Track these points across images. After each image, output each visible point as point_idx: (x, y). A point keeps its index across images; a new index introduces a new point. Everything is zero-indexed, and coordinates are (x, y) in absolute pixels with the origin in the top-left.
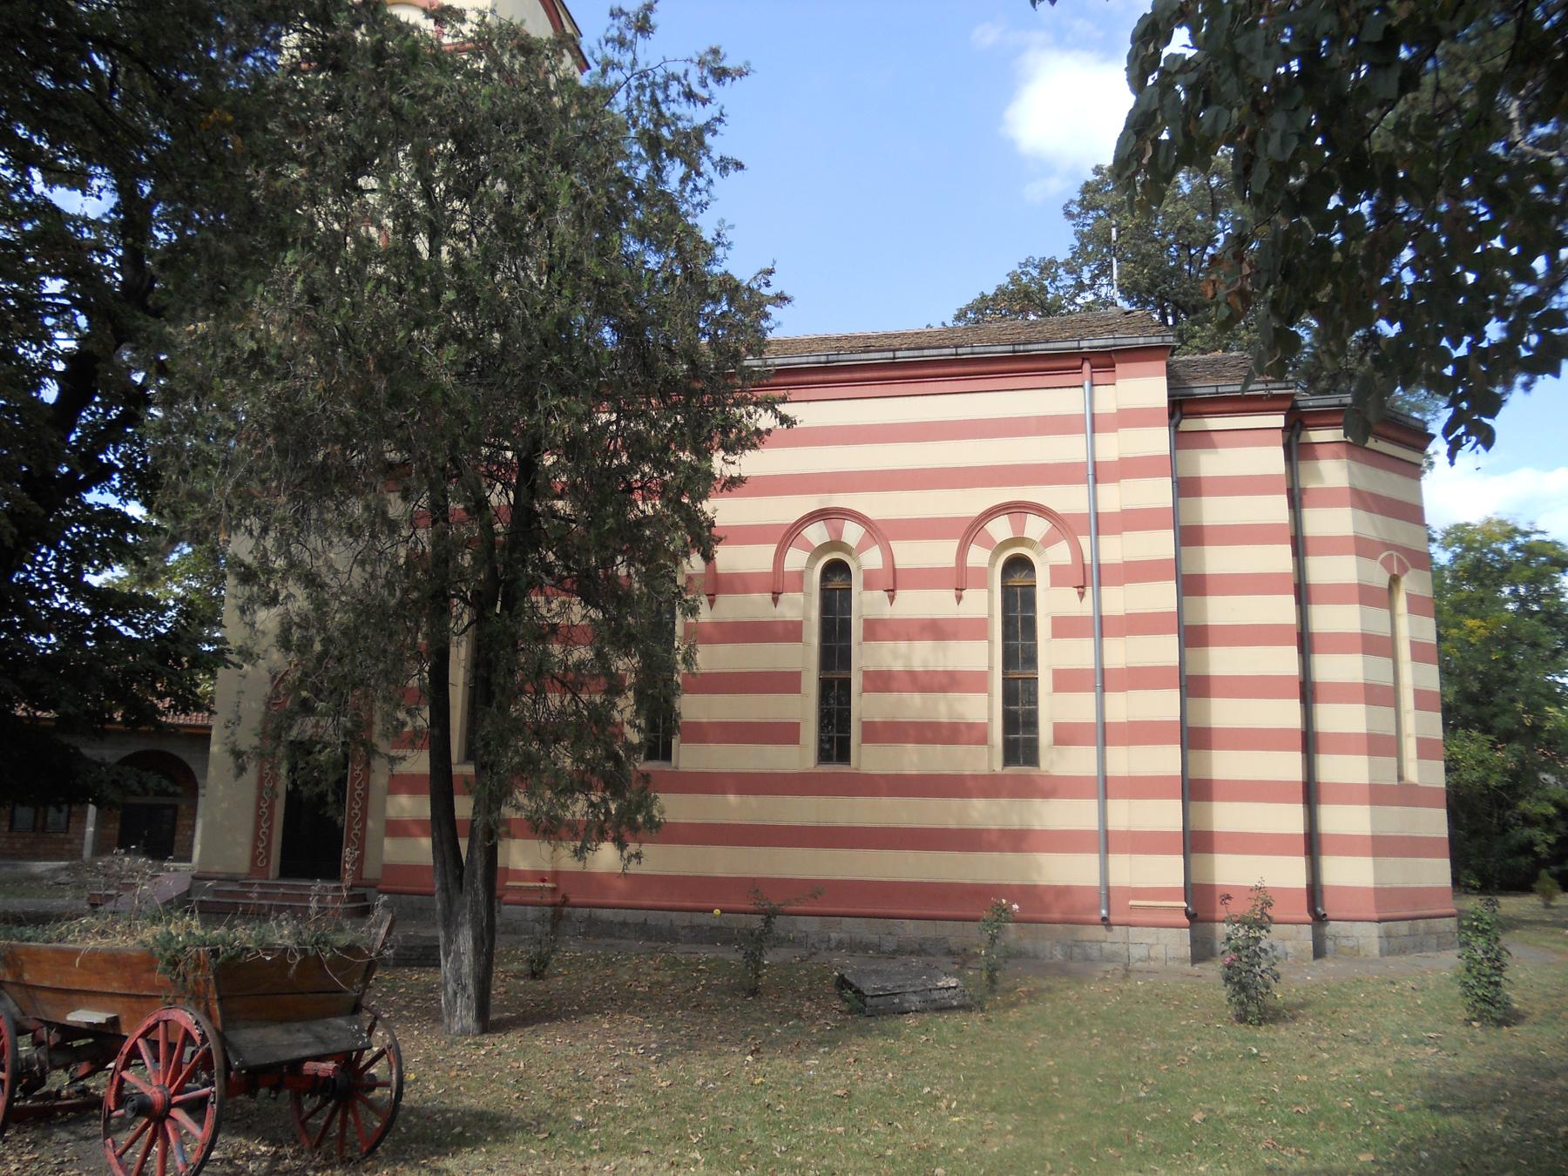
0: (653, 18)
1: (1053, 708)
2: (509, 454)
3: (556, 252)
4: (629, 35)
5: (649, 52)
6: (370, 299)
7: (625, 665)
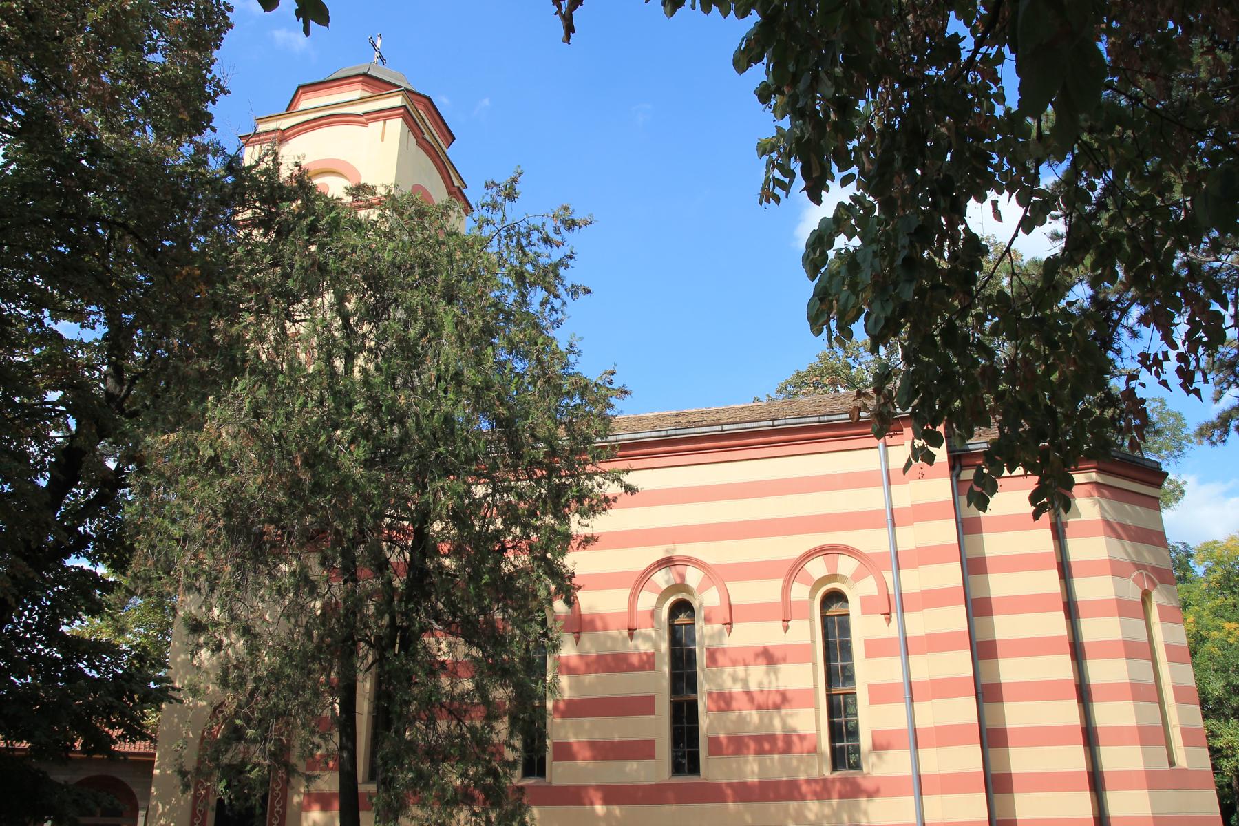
0: (518, 188)
1: (871, 719)
2: (406, 523)
3: (442, 367)
4: (500, 200)
5: (514, 213)
6: (300, 411)
7: (501, 694)
